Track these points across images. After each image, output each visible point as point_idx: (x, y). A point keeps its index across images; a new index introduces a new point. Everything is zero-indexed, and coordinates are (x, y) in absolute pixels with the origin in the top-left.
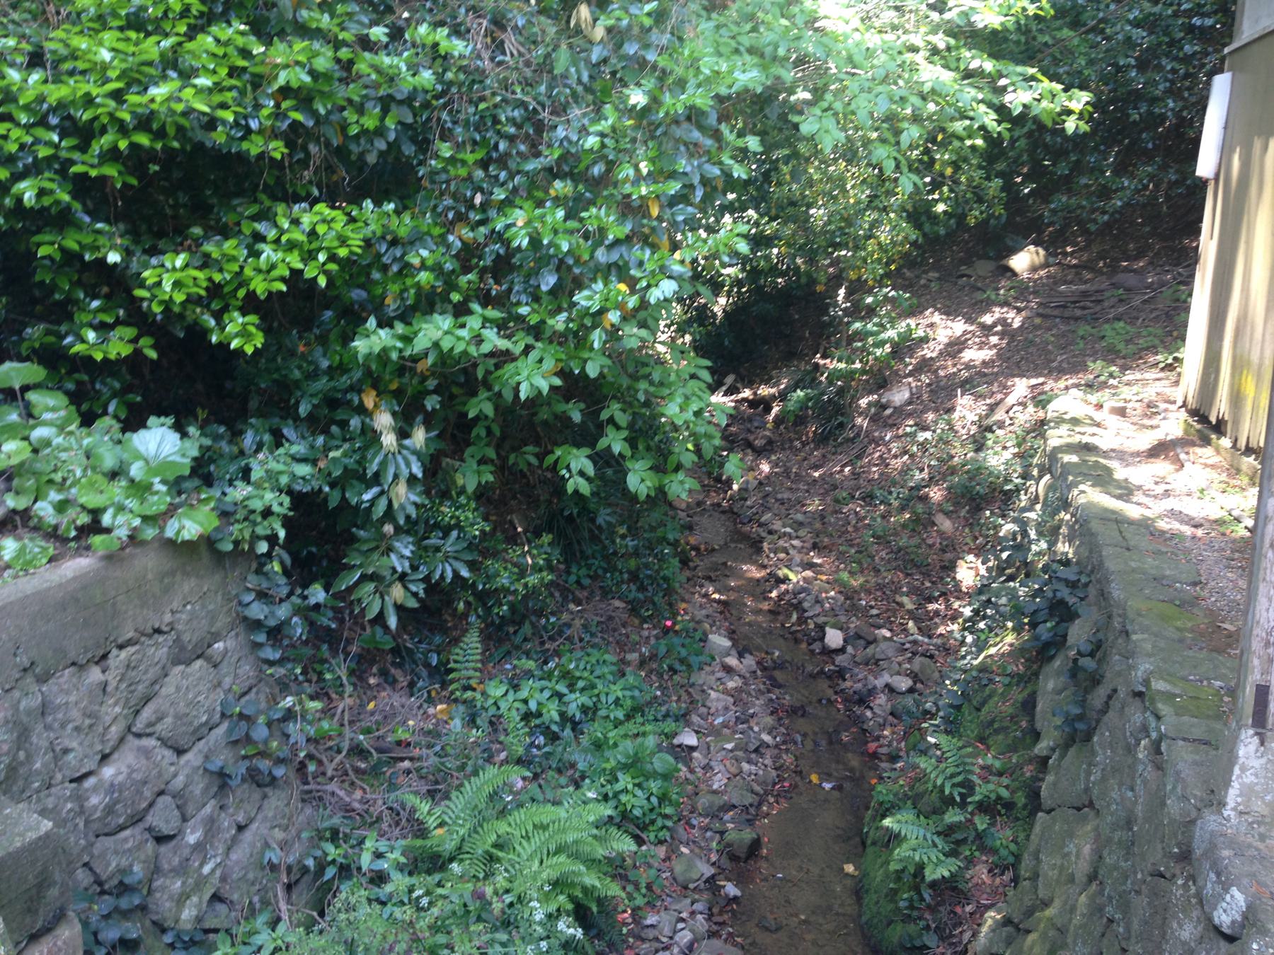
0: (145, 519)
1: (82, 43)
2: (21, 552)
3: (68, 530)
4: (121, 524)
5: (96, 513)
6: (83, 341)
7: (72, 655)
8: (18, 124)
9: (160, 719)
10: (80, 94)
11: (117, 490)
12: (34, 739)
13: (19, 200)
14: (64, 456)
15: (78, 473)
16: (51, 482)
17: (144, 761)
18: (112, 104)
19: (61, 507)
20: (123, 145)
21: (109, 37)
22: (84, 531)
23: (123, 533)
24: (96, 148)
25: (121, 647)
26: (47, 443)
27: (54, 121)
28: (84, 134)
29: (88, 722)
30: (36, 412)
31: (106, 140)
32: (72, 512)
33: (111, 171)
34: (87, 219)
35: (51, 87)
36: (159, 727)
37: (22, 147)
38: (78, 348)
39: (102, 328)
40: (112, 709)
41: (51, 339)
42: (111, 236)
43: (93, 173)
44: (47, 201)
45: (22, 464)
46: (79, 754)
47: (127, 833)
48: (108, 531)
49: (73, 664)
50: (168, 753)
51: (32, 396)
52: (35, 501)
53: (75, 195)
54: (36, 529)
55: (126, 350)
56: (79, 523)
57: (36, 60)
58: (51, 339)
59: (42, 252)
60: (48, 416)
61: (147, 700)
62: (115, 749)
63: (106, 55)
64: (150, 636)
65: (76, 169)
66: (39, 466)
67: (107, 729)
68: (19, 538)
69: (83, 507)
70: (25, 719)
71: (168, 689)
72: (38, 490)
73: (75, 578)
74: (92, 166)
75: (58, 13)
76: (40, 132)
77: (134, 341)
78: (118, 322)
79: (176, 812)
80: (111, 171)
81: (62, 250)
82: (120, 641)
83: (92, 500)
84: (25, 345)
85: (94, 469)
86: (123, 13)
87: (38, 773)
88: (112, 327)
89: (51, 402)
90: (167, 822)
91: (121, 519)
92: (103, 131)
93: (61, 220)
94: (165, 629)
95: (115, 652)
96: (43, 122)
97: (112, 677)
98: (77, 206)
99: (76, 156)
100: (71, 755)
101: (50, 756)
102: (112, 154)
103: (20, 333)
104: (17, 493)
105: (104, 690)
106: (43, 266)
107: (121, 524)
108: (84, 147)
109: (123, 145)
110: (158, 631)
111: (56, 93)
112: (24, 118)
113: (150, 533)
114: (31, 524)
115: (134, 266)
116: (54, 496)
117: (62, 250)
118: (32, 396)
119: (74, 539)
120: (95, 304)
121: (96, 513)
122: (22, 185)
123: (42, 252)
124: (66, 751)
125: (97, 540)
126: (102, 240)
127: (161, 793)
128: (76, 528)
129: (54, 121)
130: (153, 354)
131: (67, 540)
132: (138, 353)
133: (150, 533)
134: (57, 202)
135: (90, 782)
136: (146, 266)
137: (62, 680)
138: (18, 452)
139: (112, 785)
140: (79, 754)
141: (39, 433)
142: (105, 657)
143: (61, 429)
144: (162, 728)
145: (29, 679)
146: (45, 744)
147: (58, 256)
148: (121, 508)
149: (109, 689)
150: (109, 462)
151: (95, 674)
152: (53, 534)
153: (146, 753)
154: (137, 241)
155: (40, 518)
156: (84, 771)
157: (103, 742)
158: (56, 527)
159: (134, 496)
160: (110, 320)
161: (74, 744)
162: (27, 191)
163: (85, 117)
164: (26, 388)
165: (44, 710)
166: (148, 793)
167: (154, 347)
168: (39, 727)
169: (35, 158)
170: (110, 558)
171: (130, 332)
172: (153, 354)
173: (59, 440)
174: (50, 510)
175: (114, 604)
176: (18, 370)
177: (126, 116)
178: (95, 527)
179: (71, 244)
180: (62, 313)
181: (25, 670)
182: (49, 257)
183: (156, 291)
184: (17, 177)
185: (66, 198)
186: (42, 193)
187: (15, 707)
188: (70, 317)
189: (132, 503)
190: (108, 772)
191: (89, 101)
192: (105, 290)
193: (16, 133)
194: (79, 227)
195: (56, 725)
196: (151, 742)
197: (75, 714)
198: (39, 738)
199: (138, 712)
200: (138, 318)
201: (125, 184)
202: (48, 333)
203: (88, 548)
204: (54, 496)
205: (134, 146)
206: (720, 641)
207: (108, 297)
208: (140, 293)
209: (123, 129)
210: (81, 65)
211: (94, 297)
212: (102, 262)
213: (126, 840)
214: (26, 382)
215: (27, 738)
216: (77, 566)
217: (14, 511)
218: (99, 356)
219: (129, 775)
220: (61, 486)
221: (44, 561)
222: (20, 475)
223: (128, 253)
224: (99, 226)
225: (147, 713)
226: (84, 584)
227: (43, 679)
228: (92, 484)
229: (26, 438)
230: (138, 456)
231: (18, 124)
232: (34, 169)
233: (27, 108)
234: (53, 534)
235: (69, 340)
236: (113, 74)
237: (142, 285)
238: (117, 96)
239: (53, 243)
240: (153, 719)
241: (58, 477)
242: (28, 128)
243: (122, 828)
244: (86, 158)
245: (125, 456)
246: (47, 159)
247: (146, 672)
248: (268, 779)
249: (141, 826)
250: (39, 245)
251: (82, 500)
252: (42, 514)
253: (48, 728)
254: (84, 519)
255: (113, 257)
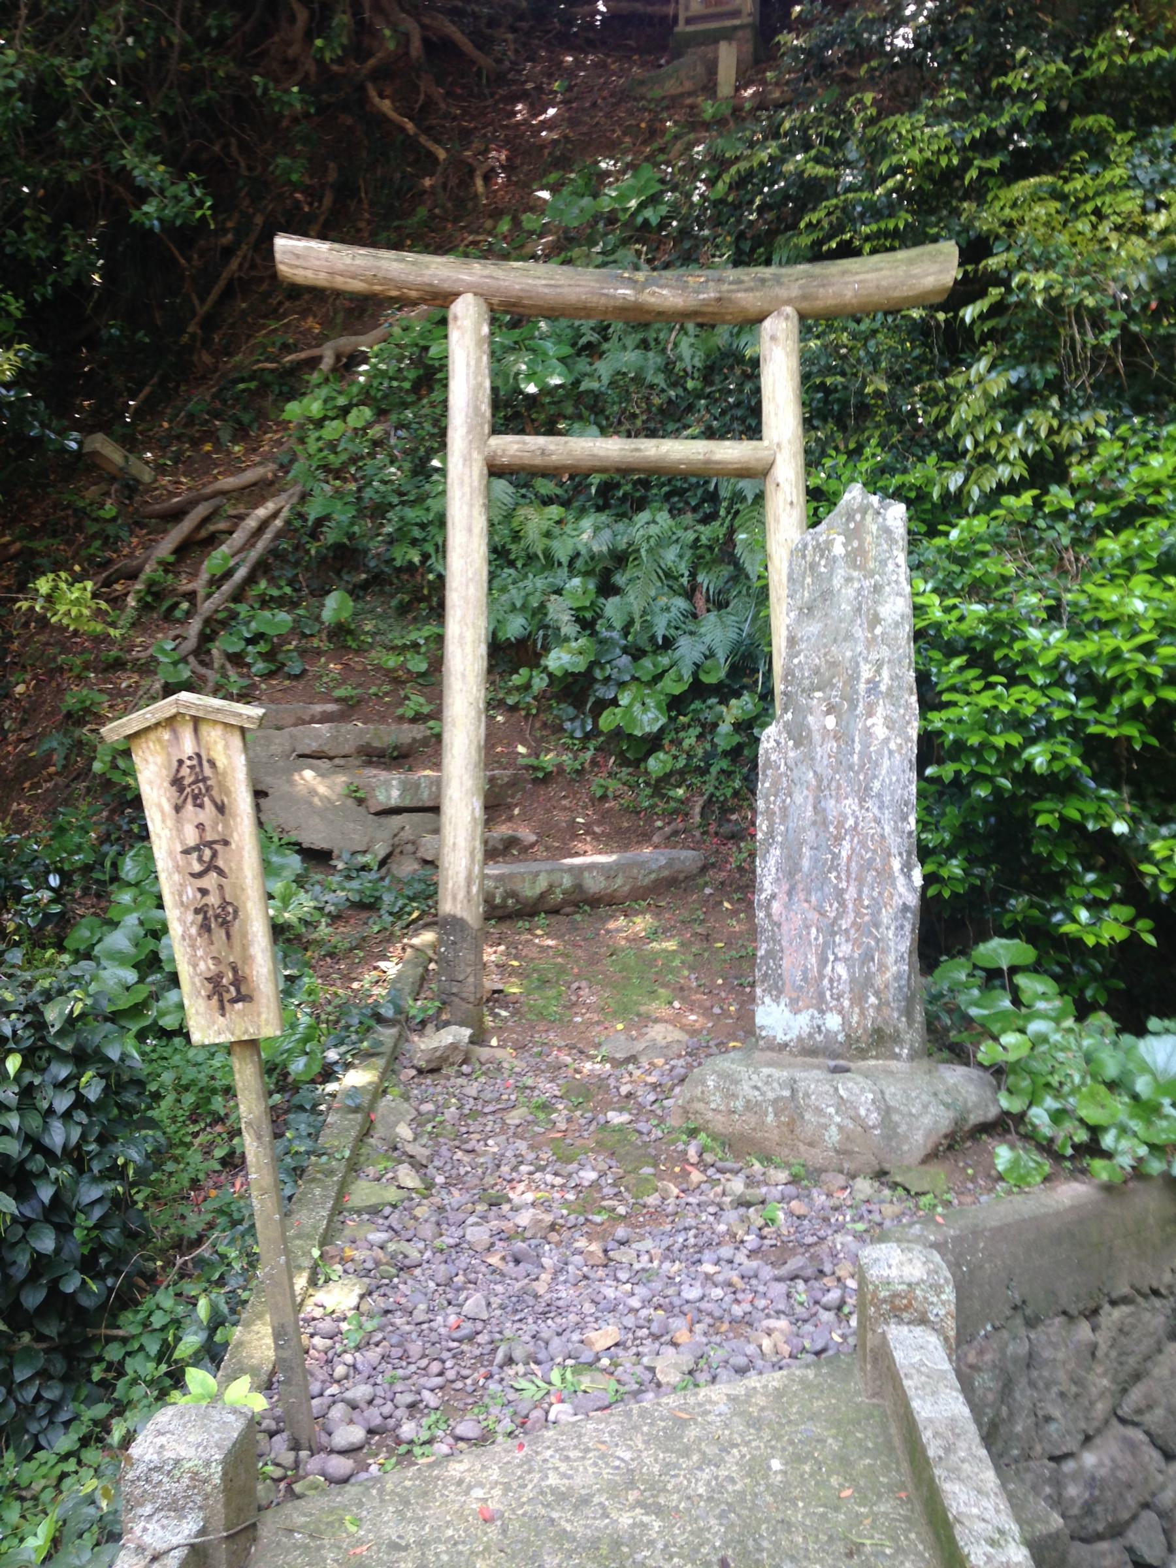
0: (1153, 1147)
1: (1111, 595)
2: (1015, 1164)
3: (1064, 1146)
4: (1126, 1150)
5: (1095, 1131)
6: (1074, 920)
7: (1064, 1302)
8: (1033, 686)
9: (1150, 1407)
10: (1107, 650)
11: (1119, 1106)
12: (1017, 1395)
13: (1029, 764)
14: (1061, 1056)
15: (1077, 1079)
16: (1048, 1085)
17: (1130, 1459)
18: (1141, 657)
19: (1057, 1117)
20: (1148, 701)
21: (1140, 583)
22: (1081, 1150)
23: (1126, 1161)
24: (1115, 707)
25: (1114, 1303)
26: (1043, 1039)
27: (1071, 679)
28: (1099, 690)
29: (1074, 1389)
30: (1025, 998)
31: (1128, 698)
32: (1069, 1125)
33: (1131, 730)
34: (1092, 785)
35: (1074, 644)
36: (1148, 1418)
37: (1040, 710)
38: (1069, 928)
39: (1095, 905)
40: (1101, 1381)
41: (1035, 913)
42: (1118, 802)
43: (1112, 734)
44: (1057, 766)
45: (1018, 1061)
46: (1061, 1430)
47: (1104, 1546)
48: (1108, 1155)
49: (1065, 1313)
50: (1156, 1455)
51: (1021, 980)
52: (1030, 1105)
53: (1085, 758)
54: (1026, 1137)
55: (1121, 934)
56: (1076, 1139)
57: (1054, 613)
58: (1035, 913)
59: (1041, 820)
60: (1041, 1005)
61: (1137, 1377)
62: (1099, 1431)
63: (1139, 606)
64: (1145, 1296)
65: (1093, 729)
66: (1036, 1065)
67: (1092, 1403)
68: (1012, 1147)
69: (1081, 1120)
70: (1011, 1368)
71: (1161, 1370)
72: (1033, 1093)
73: (1073, 1208)
74: (1112, 726)
75: (1077, 560)
76: (1057, 693)
77: (1130, 923)
78: (1115, 899)
79: (1162, 1538)
80: (1131, 730)
81: (1062, 819)
82: (1114, 1296)
83: (1093, 1115)
84: (1008, 917)
85: (1094, 1077)
86: (1155, 554)
87: (1018, 1437)
88: (1105, 905)
89: (1040, 988)
90: (1150, 1546)
91: (1124, 1144)
92: (1127, 686)
93: (1061, 785)
94: (1163, 1291)
95: (1107, 1307)
96: (1060, 683)
97: (1102, 1339)
98: (1087, 770)
99: (1092, 715)
100: (1052, 1427)
101: (1032, 1419)
102: (1135, 712)
103: (1002, 904)
104: (1010, 1092)
105: (1093, 1355)
106: (1042, 837)
107: (1126, 1150)
108: (1101, 706)
109: (1148, 701)
110: (1156, 1293)
111: (1078, 651)
112: (1040, 680)
113: (1156, 1166)
114: (1022, 1130)
115: (1141, 837)
116: (1050, 1103)
117: (1062, 819)
118: (1021, 980)
119: (1071, 1158)
120: (1090, 877)
121: (1095, 1131)
122: (1033, 750)
123: (1041, 820)
124: (1048, 1419)
125: (1098, 1164)
126: (1107, 809)
127: (1146, 1506)
128: (1074, 1147)
129: (1071, 679)
130: (1151, 940)
131: (1064, 1157)
132: (1133, 940)
133: (1156, 1166)
134: (1068, 767)
135: (1069, 1466)
136: (1154, 837)
137: (1051, 1330)
138: (1017, 1047)
139: (1093, 1478)
140: (1061, 1430)
141: (1036, 1026)
142: (1095, 1312)
143: (1057, 1021)
144: (1155, 1418)
145: (1019, 1321)
146: (1027, 1404)
147: (1056, 828)
148: (1123, 1130)
149: (1100, 1353)
150: (1111, 1071)
151: (1084, 1330)
152: (1047, 1148)
153: (1131, 1446)
154: (1144, 808)
155: (1034, 1126)
156: (1065, 1450)
157: (1087, 1419)
158: (1051, 1140)
159: (1140, 1117)
160: (1105, 896)
161: (1057, 1413)
162: (1039, 756)
163: (1109, 675)
164: (1014, 970)
165: (1031, 1361)
166: (1132, 1500)
167: (1152, 932)
168: (1023, 1381)
169: (1049, 721)
170: (1108, 1188)
171: (1126, 912)
172: (1151, 940)
173: (1056, 1037)
174: (1046, 1119)
175: (1111, 1249)
176: (1007, 947)
177: (1158, 672)
178: (1092, 1148)
179: (1074, 815)
180: (1051, 884)
181: (1015, 1308)
182: (1047, 827)
183: (1164, 867)
184: (1031, 741)
185: (1077, 762)
186: (1055, 756)
187: (1002, 1350)
188: (1060, 891)
189: (1136, 1125)
190: (1089, 1459)
191: (1116, 656)
192: (1101, 860)
193: (1032, 695)
194: (1082, 794)
195: (1041, 1384)
196: (1138, 1435)
197: (1061, 1375)
198: (1023, 1396)
199: (1124, 1391)
200: (1138, 896)
201: (1145, 746)
202: (1032, 905)
203: (1084, 1171)
204: (1050, 1103)
205: (1160, 702)
206: (514, 989)
207: (1104, 869)
208: (1147, 868)
209: (1150, 683)
210: (1104, 616)
211: (1088, 869)
212: (1106, 833)
213: (1103, 1554)
214: (1016, 962)
215: (1011, 1391)
216: (1071, 1193)
217: (1007, 1113)
218: (1090, 941)
219: (1113, 1470)
220: (1057, 1093)
221: (1039, 1179)
222: (1015, 1073)
223: (1134, 820)
224: (1104, 792)
225: (1136, 1395)
226: (1080, 1217)
227: (1032, 1323)
228: (1092, 1095)
229: (1022, 1031)
230: (1145, 1068)
231: (1033, 686)
232: (1048, 732)
233: (1047, 669)
234: (1047, 1148)
235: (1059, 917)
236: (1145, 626)
237: (1149, 858)
238: (1147, 649)
239: (1051, 812)
240: (1143, 1404)
241: (1054, 1080)
242: (1043, 689)
243: (1100, 1537)
244: (1103, 717)
245: (1131, 1066)
246: (1061, 722)
247: (1139, 1342)
248: (20, 1230)
249: (1120, 1542)
250: (1037, 813)
251: (1083, 1113)
252: (1037, 1121)
253: (1032, 1384)
254: (1082, 1136)
255: (1120, 828)
